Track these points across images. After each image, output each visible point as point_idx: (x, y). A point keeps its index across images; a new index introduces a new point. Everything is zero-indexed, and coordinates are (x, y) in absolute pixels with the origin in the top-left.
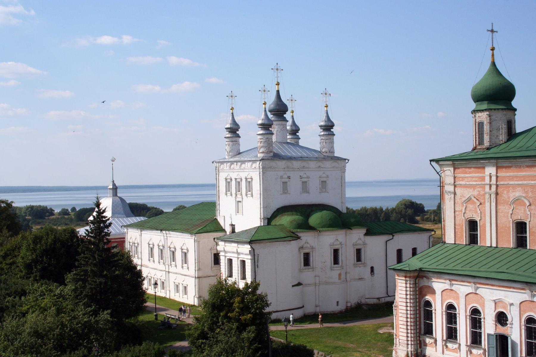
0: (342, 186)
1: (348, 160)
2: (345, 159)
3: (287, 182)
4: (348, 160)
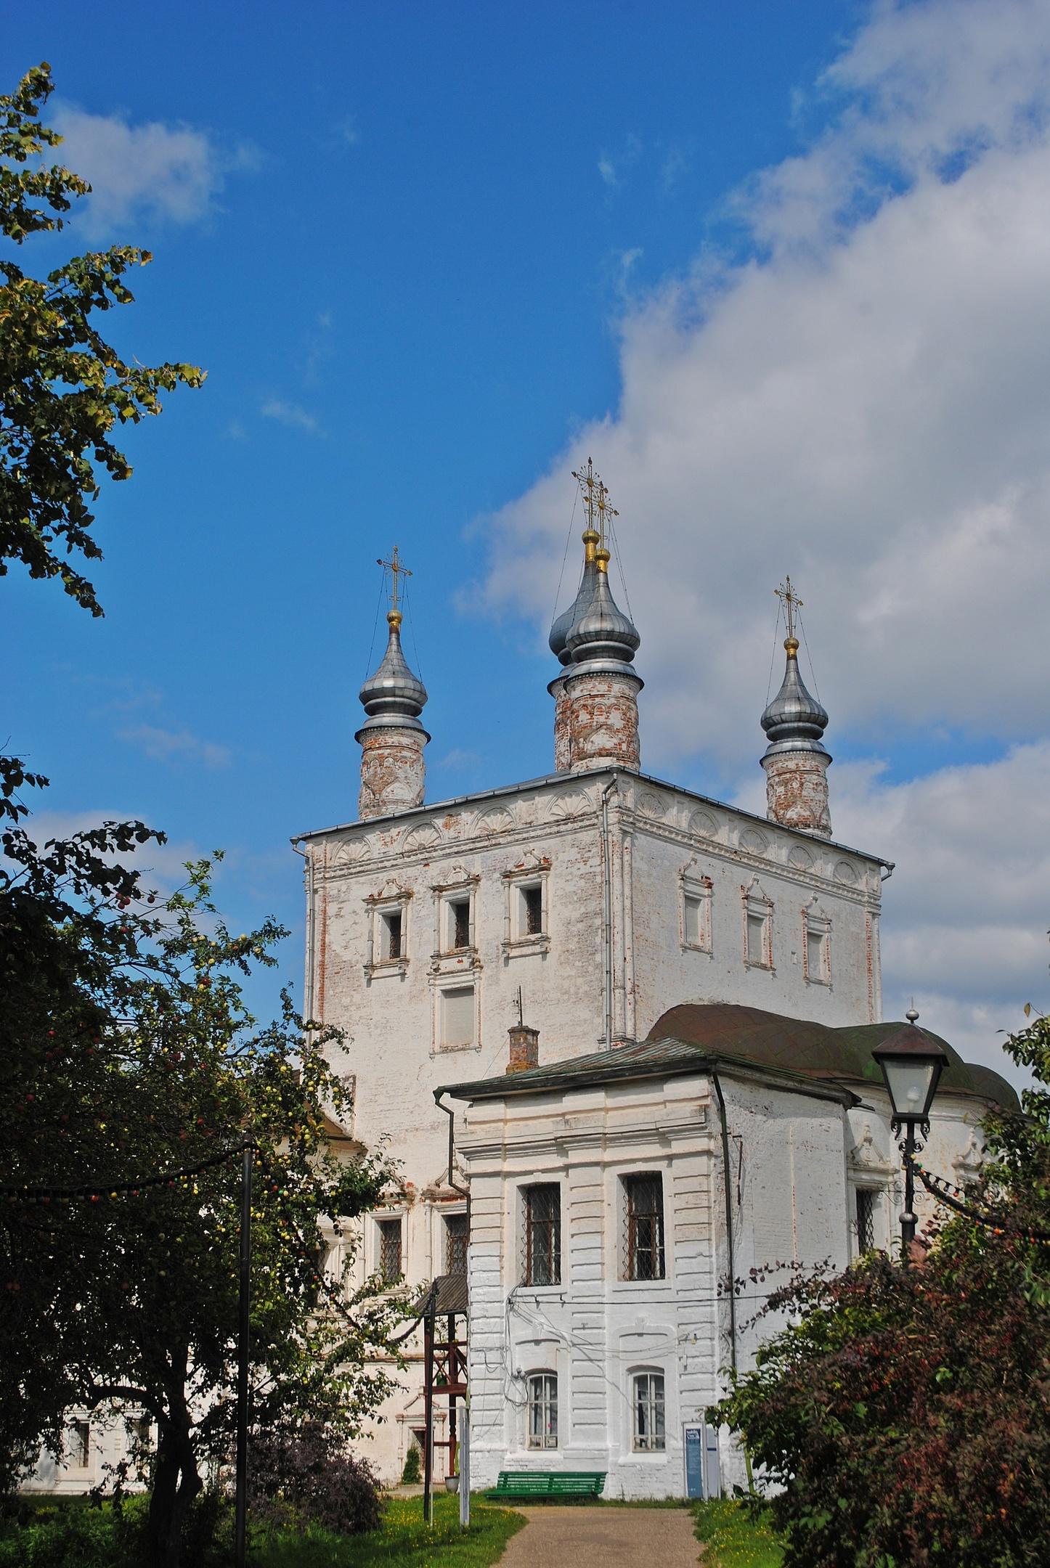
0: (869, 970)
1: (891, 867)
2: (880, 863)
3: (762, 919)
4: (891, 867)
